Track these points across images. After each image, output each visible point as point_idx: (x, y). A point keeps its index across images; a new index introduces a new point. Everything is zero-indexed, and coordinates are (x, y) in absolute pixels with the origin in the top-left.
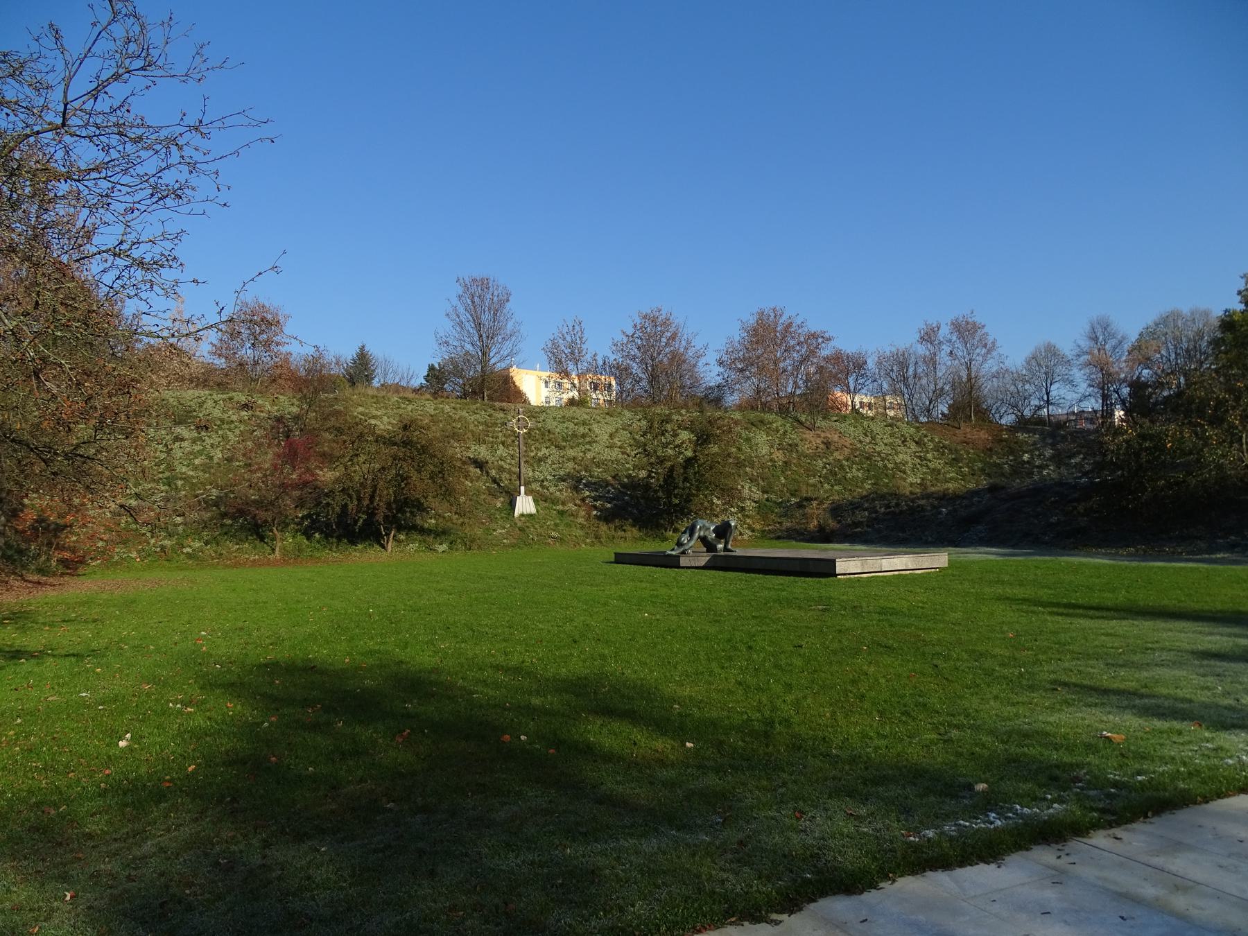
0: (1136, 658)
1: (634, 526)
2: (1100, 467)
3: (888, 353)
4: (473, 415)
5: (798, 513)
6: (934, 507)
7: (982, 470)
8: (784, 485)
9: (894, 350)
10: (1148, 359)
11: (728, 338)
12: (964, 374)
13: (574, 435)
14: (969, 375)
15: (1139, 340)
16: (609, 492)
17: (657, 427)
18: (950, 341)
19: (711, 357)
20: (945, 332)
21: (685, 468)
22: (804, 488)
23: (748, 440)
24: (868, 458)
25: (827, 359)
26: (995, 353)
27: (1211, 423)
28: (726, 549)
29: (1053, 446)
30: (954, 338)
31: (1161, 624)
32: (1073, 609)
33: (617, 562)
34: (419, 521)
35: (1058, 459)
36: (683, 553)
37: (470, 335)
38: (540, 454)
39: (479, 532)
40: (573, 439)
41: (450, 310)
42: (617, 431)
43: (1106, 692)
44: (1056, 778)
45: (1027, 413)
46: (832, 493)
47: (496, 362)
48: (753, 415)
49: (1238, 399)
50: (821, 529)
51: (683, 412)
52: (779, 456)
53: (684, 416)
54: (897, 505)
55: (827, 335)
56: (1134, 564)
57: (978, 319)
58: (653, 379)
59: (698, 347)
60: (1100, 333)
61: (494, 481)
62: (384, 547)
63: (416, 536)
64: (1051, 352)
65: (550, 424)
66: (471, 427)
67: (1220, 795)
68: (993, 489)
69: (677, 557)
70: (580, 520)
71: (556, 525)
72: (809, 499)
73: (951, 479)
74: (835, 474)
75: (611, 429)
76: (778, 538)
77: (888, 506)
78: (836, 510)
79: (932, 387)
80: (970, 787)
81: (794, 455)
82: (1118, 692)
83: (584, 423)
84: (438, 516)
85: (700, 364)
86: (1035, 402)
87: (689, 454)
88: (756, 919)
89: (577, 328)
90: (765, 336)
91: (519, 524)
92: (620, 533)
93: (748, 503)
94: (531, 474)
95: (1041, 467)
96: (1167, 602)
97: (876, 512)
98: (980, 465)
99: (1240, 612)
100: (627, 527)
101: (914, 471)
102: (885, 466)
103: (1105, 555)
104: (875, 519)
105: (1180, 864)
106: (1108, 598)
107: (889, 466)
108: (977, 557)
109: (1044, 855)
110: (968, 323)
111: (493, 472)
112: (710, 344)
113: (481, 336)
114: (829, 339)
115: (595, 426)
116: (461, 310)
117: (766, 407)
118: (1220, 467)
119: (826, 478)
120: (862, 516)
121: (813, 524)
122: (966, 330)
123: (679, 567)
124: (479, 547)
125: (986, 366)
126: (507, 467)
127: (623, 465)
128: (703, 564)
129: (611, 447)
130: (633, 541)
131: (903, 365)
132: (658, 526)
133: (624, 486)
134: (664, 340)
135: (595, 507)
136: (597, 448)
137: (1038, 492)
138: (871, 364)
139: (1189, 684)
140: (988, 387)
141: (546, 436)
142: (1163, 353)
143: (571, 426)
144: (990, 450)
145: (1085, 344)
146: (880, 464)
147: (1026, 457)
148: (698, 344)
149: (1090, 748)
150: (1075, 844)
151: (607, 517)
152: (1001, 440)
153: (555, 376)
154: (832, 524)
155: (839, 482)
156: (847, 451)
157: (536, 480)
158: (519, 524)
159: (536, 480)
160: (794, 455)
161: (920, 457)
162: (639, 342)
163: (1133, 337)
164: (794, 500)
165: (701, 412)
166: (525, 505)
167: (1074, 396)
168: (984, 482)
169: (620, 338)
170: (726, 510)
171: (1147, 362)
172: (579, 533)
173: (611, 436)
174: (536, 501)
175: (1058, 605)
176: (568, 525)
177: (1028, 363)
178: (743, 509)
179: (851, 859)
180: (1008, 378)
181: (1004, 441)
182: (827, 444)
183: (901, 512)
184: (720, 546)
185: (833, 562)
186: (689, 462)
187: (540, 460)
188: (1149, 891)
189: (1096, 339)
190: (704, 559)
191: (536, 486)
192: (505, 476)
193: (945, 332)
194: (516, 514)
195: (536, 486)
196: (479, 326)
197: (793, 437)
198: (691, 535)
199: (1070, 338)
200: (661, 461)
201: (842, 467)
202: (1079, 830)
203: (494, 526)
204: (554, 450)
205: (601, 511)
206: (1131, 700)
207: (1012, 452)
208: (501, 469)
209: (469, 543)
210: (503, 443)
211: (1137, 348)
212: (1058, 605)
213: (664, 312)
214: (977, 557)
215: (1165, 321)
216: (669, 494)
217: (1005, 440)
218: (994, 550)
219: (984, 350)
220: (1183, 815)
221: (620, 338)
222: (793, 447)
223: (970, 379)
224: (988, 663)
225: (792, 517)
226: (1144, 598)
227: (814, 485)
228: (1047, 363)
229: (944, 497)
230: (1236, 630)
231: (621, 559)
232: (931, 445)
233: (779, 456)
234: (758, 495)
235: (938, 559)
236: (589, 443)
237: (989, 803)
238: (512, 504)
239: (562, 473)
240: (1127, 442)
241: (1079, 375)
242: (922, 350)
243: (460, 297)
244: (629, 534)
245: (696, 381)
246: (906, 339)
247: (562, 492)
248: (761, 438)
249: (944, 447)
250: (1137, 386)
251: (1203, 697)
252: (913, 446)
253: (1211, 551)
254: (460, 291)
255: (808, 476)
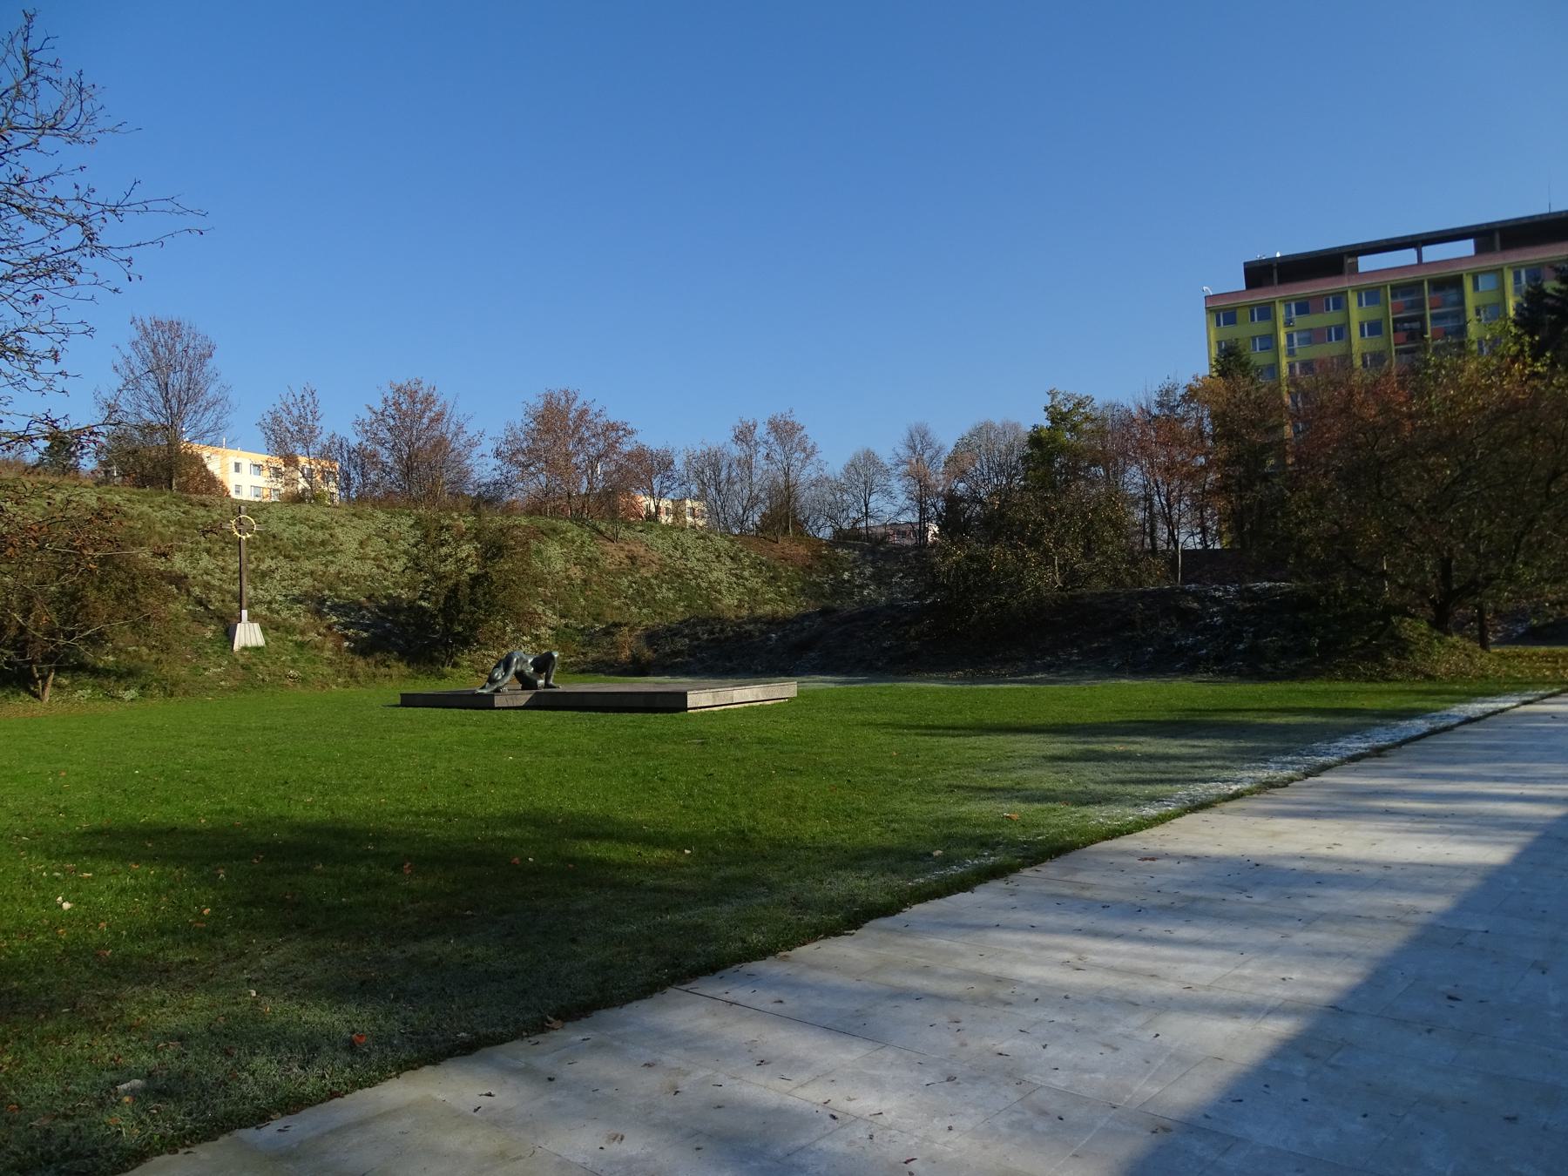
0: (1005, 763)
1: (400, 660)
2: (933, 587)
3: (698, 453)
4: (152, 511)
5: (605, 642)
6: (762, 632)
7: (802, 590)
8: (584, 608)
9: (705, 448)
10: (964, 472)
11: (508, 423)
12: (781, 480)
13: (310, 543)
14: (787, 481)
15: (954, 452)
16: (363, 617)
17: (431, 535)
18: (766, 442)
19: (488, 447)
20: (761, 431)
21: (472, 587)
22: (608, 612)
23: (539, 552)
24: (679, 576)
25: (630, 456)
26: (814, 459)
27: (1029, 546)
28: (547, 685)
29: (873, 563)
30: (772, 440)
31: (1011, 738)
32: (932, 729)
33: (403, 705)
34: (89, 657)
35: (880, 578)
36: (497, 691)
37: (150, 398)
38: (263, 567)
39: (184, 672)
40: (308, 547)
41: (119, 361)
42: (369, 538)
43: (991, 790)
44: (985, 843)
45: (846, 526)
46: (643, 617)
47: (189, 442)
48: (542, 522)
49: (1052, 521)
50: (635, 660)
51: (455, 515)
52: (576, 572)
53: (464, 522)
54: (722, 630)
55: (629, 427)
56: (967, 687)
57: (798, 419)
58: (409, 469)
59: (470, 434)
60: (918, 441)
61: (200, 602)
62: (36, 696)
63: (84, 678)
64: (870, 459)
65: (275, 527)
66: (158, 527)
67: (1092, 843)
68: (825, 612)
69: (491, 697)
70: (327, 654)
71: (294, 661)
72: (617, 625)
73: (771, 600)
74: (642, 595)
75: (360, 535)
76: (583, 672)
77: (711, 632)
78: (652, 637)
79: (746, 492)
80: (930, 855)
81: (594, 572)
82: (1002, 789)
83: (323, 527)
84: (116, 651)
85: (474, 455)
86: (854, 514)
87: (472, 570)
88: (836, 935)
89: (308, 399)
90: (555, 423)
91: (242, 660)
92: (383, 670)
93: (543, 629)
94: (252, 593)
95: (862, 587)
96: (1008, 718)
97: (698, 639)
98: (799, 584)
99: (1069, 725)
100: (392, 662)
101: (734, 590)
102: (698, 585)
103: (937, 680)
104: (697, 647)
105: (1080, 877)
106: (958, 719)
107: (704, 585)
108: (816, 686)
109: (999, 884)
110: (786, 423)
111: (197, 591)
112: (485, 429)
113: (168, 401)
114: (631, 433)
115: (338, 531)
116: (136, 361)
117: (557, 512)
118: (1037, 589)
119: (632, 599)
120: (682, 643)
121: (625, 655)
122: (784, 431)
123: (494, 708)
124: (186, 692)
125: (805, 472)
126: (217, 583)
127: (380, 582)
128: (522, 703)
129: (362, 558)
130: (398, 679)
131: (716, 468)
132: (433, 661)
133: (383, 609)
134: (425, 421)
135: (347, 638)
136: (342, 559)
137: (869, 614)
138: (679, 464)
139: (1049, 779)
140: (806, 496)
141: (268, 541)
142: (977, 467)
143: (305, 529)
144: (810, 567)
145: (904, 452)
146: (693, 583)
147: (846, 576)
148: (471, 430)
149: (998, 824)
150: (1012, 877)
151: (363, 649)
152: (821, 557)
153: (278, 462)
154: (648, 654)
155: (647, 604)
156: (655, 568)
157: (260, 602)
158: (242, 660)
159: (260, 602)
160: (594, 572)
161: (736, 575)
162: (392, 423)
163: (950, 448)
164: (598, 626)
165: (479, 516)
166: (248, 634)
167: (891, 507)
168: (811, 607)
169: (367, 416)
170: (517, 639)
171: (962, 475)
172: (328, 670)
173: (361, 543)
174: (264, 630)
175: (918, 727)
176: (312, 661)
177: (847, 471)
178: (537, 638)
179: (880, 898)
180: (826, 488)
181: (823, 557)
182: (632, 559)
183: (727, 638)
184: (541, 682)
185: (685, 694)
186: (476, 580)
187: (264, 575)
188: (1068, 891)
189: (913, 448)
190: (524, 697)
191: (261, 610)
192: (214, 595)
193: (761, 431)
194: (236, 647)
195: (261, 610)
196: (164, 388)
197: (592, 550)
198: (507, 669)
199: (889, 448)
200: (440, 578)
201: (650, 586)
202: (1013, 869)
203: (203, 663)
204: (283, 562)
205: (355, 642)
206: (1014, 792)
207: (832, 570)
208: (207, 586)
209: (170, 688)
210: (208, 551)
211: (952, 460)
212: (918, 727)
213: (425, 386)
214: (816, 686)
215: (978, 432)
216: (450, 620)
217: (825, 557)
218: (828, 678)
219: (803, 455)
220: (1072, 855)
221: (367, 416)
222: (592, 561)
223: (788, 488)
224: (890, 776)
225: (598, 646)
226: (989, 716)
227: (619, 608)
228: (865, 471)
229: (773, 622)
230: (1070, 738)
231: (408, 701)
232: (747, 562)
233: (576, 572)
234: (554, 620)
235: (785, 689)
236: (332, 553)
237: (947, 861)
238: (230, 634)
239: (296, 592)
240: (957, 563)
241: (897, 486)
242: (736, 451)
243: (135, 344)
244: (394, 671)
245: (464, 475)
246: (717, 436)
247: (300, 617)
248: (554, 550)
249: (762, 563)
250: (952, 499)
251: (1061, 787)
252: (728, 562)
253: (1030, 671)
254: (136, 335)
255: (612, 597)
